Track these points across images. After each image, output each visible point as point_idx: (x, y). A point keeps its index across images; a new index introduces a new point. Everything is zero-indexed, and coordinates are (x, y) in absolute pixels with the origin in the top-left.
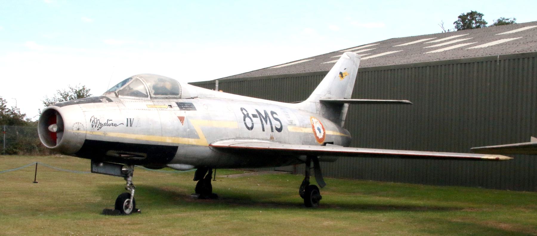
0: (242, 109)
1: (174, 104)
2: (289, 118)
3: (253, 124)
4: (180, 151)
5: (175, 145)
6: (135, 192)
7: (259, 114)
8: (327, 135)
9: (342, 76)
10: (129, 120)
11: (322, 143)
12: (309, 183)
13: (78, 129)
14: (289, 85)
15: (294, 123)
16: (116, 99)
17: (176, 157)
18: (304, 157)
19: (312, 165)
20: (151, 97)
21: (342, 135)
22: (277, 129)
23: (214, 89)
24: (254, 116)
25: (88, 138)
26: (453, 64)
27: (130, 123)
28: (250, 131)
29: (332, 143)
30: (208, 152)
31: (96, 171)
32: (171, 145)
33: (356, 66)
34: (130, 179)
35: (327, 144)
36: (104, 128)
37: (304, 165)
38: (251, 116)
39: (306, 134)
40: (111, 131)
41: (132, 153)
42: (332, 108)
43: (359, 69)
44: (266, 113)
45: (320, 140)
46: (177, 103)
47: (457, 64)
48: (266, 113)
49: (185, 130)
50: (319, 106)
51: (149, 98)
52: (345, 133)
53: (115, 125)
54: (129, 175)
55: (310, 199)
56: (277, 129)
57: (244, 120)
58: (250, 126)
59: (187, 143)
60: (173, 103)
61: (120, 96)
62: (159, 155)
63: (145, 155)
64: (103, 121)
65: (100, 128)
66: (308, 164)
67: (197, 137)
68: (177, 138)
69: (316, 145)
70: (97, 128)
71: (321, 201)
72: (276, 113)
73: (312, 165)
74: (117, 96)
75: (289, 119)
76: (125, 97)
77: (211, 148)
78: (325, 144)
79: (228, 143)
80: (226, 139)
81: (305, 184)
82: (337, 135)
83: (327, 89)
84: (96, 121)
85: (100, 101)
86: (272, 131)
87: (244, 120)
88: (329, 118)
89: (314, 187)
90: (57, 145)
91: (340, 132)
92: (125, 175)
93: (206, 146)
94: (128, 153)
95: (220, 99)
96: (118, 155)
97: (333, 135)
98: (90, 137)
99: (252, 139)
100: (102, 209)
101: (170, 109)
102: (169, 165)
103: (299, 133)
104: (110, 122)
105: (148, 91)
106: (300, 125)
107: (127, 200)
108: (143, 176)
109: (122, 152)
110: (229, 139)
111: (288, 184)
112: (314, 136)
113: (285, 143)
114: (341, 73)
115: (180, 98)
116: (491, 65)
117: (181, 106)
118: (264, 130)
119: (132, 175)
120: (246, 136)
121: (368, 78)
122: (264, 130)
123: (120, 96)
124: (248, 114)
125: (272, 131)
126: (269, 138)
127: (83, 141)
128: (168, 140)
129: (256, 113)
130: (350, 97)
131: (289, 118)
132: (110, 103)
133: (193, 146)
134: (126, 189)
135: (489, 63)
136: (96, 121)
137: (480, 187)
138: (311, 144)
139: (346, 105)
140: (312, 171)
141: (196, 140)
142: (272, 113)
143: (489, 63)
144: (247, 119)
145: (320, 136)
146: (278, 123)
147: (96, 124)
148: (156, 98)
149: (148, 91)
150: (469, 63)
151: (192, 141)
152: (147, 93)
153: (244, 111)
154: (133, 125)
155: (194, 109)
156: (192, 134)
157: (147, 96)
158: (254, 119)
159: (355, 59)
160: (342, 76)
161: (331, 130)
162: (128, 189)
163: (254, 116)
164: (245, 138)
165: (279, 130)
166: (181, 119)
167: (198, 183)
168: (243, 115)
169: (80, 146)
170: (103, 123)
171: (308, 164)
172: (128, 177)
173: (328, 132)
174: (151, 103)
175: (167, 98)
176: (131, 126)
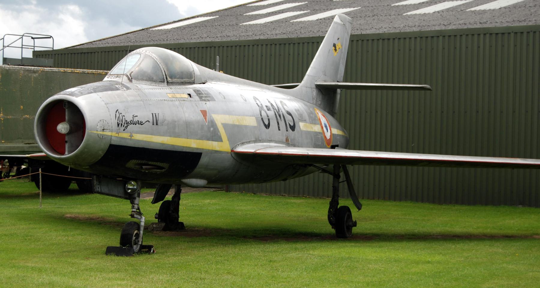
4: (203, 160)
10: (154, 115)
17: (197, 170)
20: (168, 82)
25: (113, 143)
26: (479, 35)
28: (267, 130)
30: (229, 161)
32: (195, 151)
42: (327, 94)
43: (352, 36)
45: (328, 141)
46: (195, 91)
47: (485, 34)
50: (315, 92)
53: (141, 123)
54: (136, 195)
55: (342, 228)
59: (210, 148)
63: (166, 165)
64: (129, 118)
71: (355, 230)
77: (233, 155)
83: (322, 67)
84: (121, 118)
85: (117, 89)
90: (67, 155)
91: (343, 131)
93: (228, 153)
94: (150, 163)
97: (338, 135)
98: (115, 142)
100: (105, 249)
101: (191, 99)
104: (136, 119)
105: (163, 71)
107: (136, 232)
109: (144, 162)
114: (335, 45)
115: (193, 83)
116: (534, 37)
121: (362, 49)
122: (279, 130)
125: (153, 124)
127: (107, 147)
129: (269, 105)
133: (217, 152)
135: (531, 34)
136: (121, 118)
137: (521, 206)
138: (316, 146)
139: (339, 91)
143: (531, 34)
150: (503, 34)
154: (159, 122)
161: (325, 125)
167: (338, 204)
169: (101, 154)
170: (129, 121)
171: (337, 177)
172: (135, 198)
176: (157, 124)
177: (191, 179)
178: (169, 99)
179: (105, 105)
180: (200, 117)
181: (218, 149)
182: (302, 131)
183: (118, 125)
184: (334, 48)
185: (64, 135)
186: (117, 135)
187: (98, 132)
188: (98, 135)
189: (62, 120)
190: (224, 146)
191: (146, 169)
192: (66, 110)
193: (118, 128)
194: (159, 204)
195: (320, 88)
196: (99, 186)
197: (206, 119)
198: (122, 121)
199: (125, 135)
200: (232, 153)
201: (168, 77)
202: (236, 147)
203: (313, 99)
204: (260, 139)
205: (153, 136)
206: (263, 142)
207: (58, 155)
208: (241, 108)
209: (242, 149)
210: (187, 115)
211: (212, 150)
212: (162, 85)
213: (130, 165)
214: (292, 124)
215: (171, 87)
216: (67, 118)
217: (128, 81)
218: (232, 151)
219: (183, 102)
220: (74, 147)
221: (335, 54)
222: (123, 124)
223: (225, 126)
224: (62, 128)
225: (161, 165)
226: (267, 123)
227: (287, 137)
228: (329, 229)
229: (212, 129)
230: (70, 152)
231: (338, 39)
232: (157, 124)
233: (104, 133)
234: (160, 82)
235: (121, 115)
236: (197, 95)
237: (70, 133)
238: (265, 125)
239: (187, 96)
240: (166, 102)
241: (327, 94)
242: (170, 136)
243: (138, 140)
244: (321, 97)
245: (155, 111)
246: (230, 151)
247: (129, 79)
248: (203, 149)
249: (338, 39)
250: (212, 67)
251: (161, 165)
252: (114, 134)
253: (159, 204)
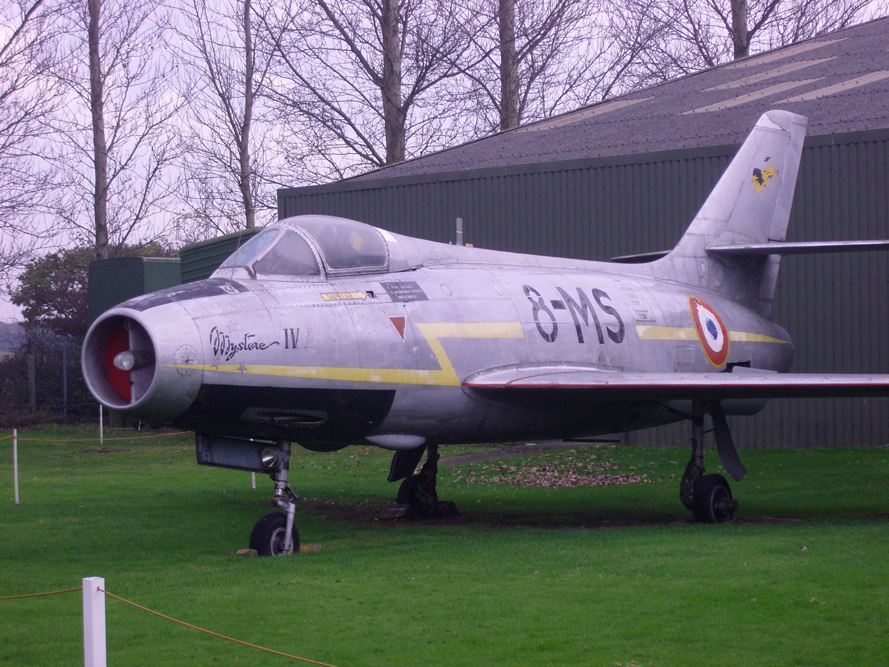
0: (527, 290)
1: (377, 287)
2: (637, 303)
3: (555, 328)
4: (398, 402)
5: (388, 388)
6: (297, 509)
7: (569, 300)
8: (734, 343)
9: (760, 181)
11: (723, 365)
12: (702, 470)
13: (187, 361)
14: (598, 193)
15: (649, 316)
16: (253, 282)
17: (390, 419)
18: (685, 404)
19: (708, 420)
20: (327, 275)
21: (769, 339)
22: (612, 335)
23: (454, 243)
24: (557, 305)
25: (208, 381)
27: (292, 341)
28: (551, 344)
29: (747, 364)
30: (460, 402)
31: (209, 459)
32: (379, 388)
33: (795, 146)
34: (283, 475)
35: (735, 368)
36: (239, 354)
37: (687, 423)
38: (550, 306)
39: (681, 345)
40: (254, 363)
41: (298, 411)
42: (741, 270)
44: (583, 297)
45: (717, 358)
46: (384, 285)
48: (583, 297)
49: (408, 347)
50: (705, 266)
51: (322, 277)
52: (776, 335)
53: (262, 347)
55: (707, 504)
56: (612, 335)
57: (536, 318)
58: (549, 331)
59: (414, 382)
60: (375, 283)
61: (259, 276)
62: (343, 414)
64: (237, 340)
65: (232, 354)
66: (698, 422)
67: (434, 365)
68: (391, 371)
69: (710, 370)
70: (225, 357)
72: (605, 295)
73: (708, 420)
74: (253, 276)
75: (637, 308)
76: (273, 277)
77: (467, 391)
78: (729, 368)
79: (502, 377)
80: (499, 368)
81: (693, 470)
82: (756, 343)
84: (221, 340)
85: (221, 292)
86: (601, 341)
87: (536, 318)
88: (733, 300)
89: (720, 480)
90: (134, 403)
92: (272, 471)
93: (454, 388)
94: (288, 411)
95: (474, 264)
96: (268, 419)
97: (747, 343)
99: (560, 363)
101: (373, 300)
102: (371, 438)
103: (661, 343)
104: (250, 341)
105: (318, 260)
106: (651, 314)
108: (310, 469)
110: (504, 367)
111: (648, 468)
112: (702, 349)
113: (631, 370)
114: (757, 172)
115: (387, 271)
117: (395, 291)
118: (581, 340)
119: (287, 467)
120: (541, 356)
122: (581, 340)
123: (259, 276)
124: (541, 300)
125: (601, 341)
126: (594, 359)
127: (197, 387)
128: (373, 377)
129: (559, 298)
130: (783, 235)
131: (637, 303)
132: (245, 295)
134: (275, 504)
136: (221, 340)
138: (680, 367)
139: (776, 258)
140: (710, 437)
141: (434, 373)
142: (597, 293)
144: (542, 314)
145: (716, 345)
146: (613, 319)
147: (224, 349)
148: (337, 276)
149: (318, 260)
151: (423, 376)
152: (317, 264)
153: (532, 294)
154: (298, 344)
155: (422, 297)
156: (422, 357)
157: (317, 273)
158: (557, 313)
159: (792, 130)
160: (760, 181)
161: (746, 333)
162: (280, 503)
163: (557, 305)
164: (539, 363)
165: (617, 337)
166: (399, 323)
168: (530, 306)
170: (236, 343)
171: (698, 422)
172: (279, 471)
173: (737, 336)
174: (326, 288)
175: (360, 274)
176: (294, 347)
177: (391, 436)
178: (324, 303)
179: (192, 321)
180: (391, 332)
181: (431, 382)
182: (641, 342)
183: (216, 352)
184: (756, 178)
185: (127, 373)
186: (214, 369)
187: (178, 366)
188: (178, 370)
189: (125, 348)
190: (447, 376)
191: (280, 421)
192: (130, 332)
193: (215, 358)
194: (398, 484)
195: (718, 257)
196: (208, 453)
197: (402, 334)
198: (223, 344)
199: (229, 368)
200: (465, 388)
201: (326, 265)
202: (472, 377)
203: (701, 278)
204: (532, 360)
205: (288, 367)
206: (539, 366)
207: (113, 404)
208: (485, 311)
209: (481, 380)
210: (359, 328)
211: (418, 385)
212: (315, 279)
213: (233, 415)
214: (616, 330)
215: (333, 282)
216: (131, 345)
217: (248, 277)
218: (464, 384)
219: (352, 306)
220: (143, 389)
221: (760, 188)
222: (225, 350)
223: (446, 343)
224: (124, 361)
225: (313, 413)
226: (549, 331)
227: (601, 354)
228: (689, 514)
229: (415, 349)
230: (137, 399)
231: (767, 159)
232: (294, 347)
233: (189, 367)
234: (311, 274)
235: (221, 336)
236: (389, 293)
237: (136, 367)
238: (545, 335)
239: (364, 296)
240: (316, 309)
241: (741, 270)
242: (324, 365)
243: (258, 375)
244: (721, 272)
245: (292, 324)
246: (459, 384)
247: (250, 273)
248: (396, 384)
249: (767, 159)
250: (447, 237)
251: (313, 413)
252: (208, 367)
253: (398, 484)
